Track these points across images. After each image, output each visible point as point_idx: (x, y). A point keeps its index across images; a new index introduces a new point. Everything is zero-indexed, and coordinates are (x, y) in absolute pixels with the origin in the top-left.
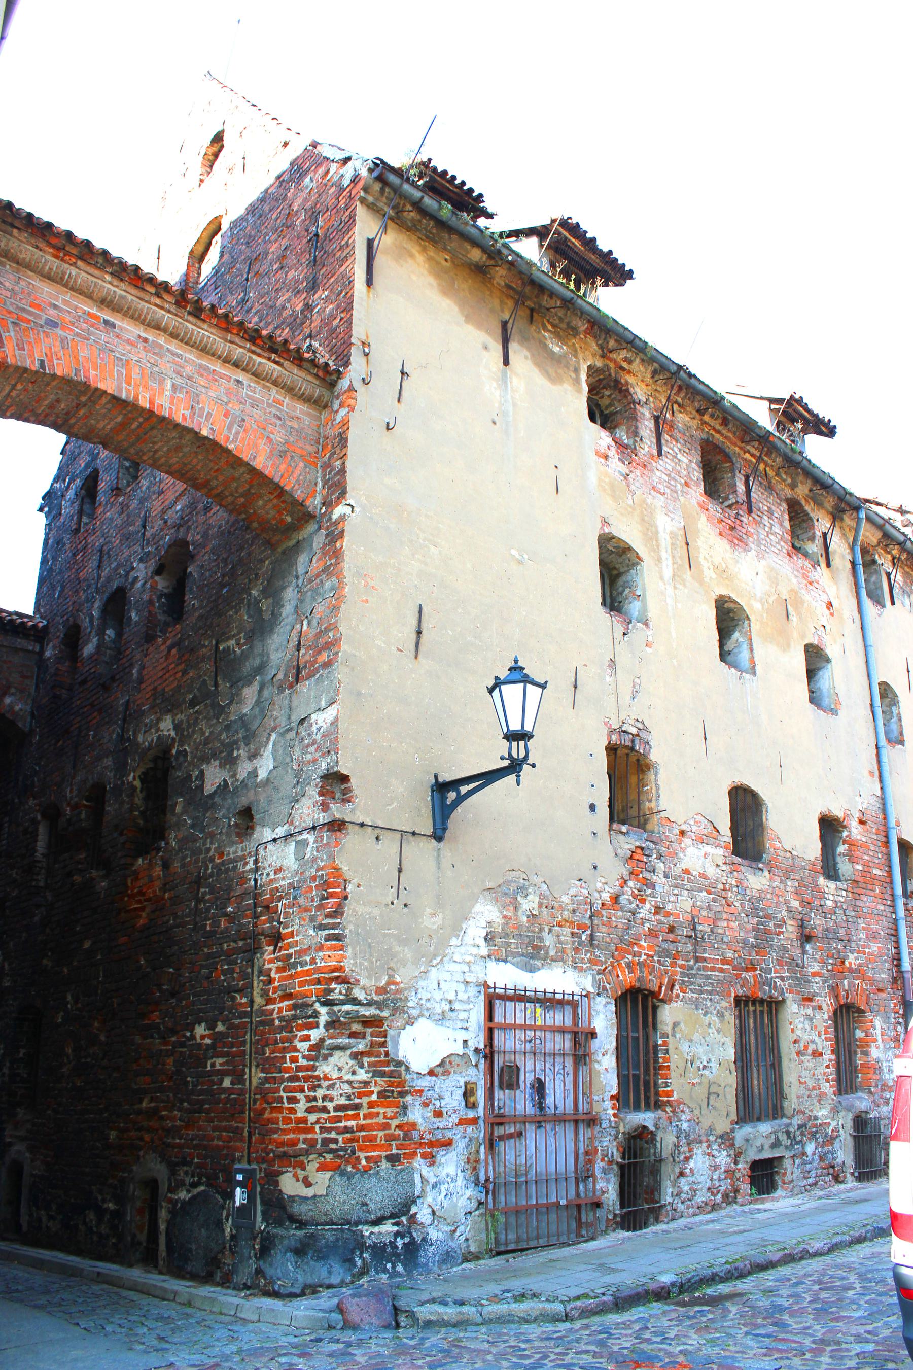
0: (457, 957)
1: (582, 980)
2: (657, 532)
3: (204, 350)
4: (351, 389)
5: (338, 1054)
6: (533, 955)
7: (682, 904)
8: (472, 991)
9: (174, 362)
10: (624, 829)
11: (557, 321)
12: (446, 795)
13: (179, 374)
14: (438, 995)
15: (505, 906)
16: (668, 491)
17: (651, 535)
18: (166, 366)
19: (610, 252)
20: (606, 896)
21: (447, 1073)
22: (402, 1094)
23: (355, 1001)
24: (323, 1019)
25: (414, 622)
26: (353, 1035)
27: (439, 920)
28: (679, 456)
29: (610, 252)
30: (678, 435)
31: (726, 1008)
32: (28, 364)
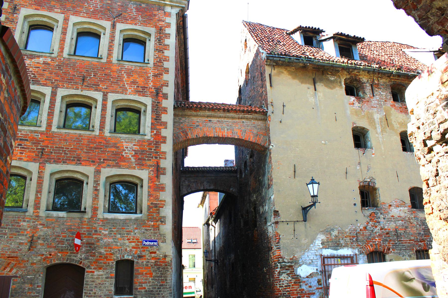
0: (313, 249)
1: (355, 251)
2: (374, 120)
3: (233, 118)
4: (269, 116)
5: (283, 274)
6: (337, 246)
7: (391, 226)
8: (318, 257)
9: (226, 123)
10: (366, 208)
11: (331, 71)
12: (305, 210)
13: (228, 126)
14: (308, 259)
15: (327, 235)
16: (378, 106)
17: (371, 120)
18: (225, 125)
19: (355, 36)
20: (362, 227)
21: (312, 277)
22: (300, 282)
23: (285, 262)
24: (279, 266)
25: (293, 169)
26: (286, 270)
27: (307, 241)
28: (382, 93)
29: (355, 36)
30: (381, 87)
31: (412, 254)
32: (194, 137)
